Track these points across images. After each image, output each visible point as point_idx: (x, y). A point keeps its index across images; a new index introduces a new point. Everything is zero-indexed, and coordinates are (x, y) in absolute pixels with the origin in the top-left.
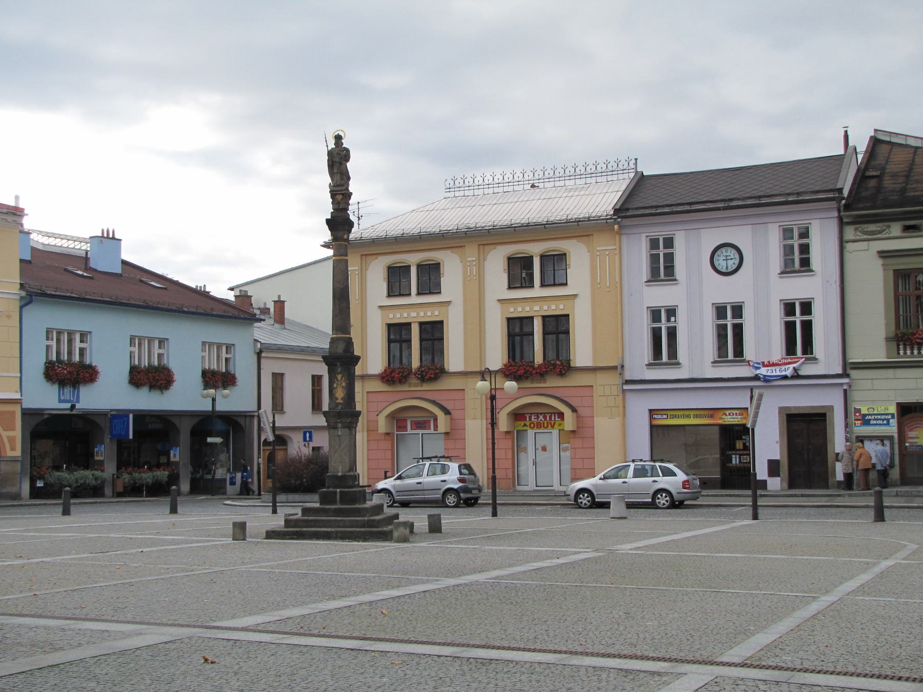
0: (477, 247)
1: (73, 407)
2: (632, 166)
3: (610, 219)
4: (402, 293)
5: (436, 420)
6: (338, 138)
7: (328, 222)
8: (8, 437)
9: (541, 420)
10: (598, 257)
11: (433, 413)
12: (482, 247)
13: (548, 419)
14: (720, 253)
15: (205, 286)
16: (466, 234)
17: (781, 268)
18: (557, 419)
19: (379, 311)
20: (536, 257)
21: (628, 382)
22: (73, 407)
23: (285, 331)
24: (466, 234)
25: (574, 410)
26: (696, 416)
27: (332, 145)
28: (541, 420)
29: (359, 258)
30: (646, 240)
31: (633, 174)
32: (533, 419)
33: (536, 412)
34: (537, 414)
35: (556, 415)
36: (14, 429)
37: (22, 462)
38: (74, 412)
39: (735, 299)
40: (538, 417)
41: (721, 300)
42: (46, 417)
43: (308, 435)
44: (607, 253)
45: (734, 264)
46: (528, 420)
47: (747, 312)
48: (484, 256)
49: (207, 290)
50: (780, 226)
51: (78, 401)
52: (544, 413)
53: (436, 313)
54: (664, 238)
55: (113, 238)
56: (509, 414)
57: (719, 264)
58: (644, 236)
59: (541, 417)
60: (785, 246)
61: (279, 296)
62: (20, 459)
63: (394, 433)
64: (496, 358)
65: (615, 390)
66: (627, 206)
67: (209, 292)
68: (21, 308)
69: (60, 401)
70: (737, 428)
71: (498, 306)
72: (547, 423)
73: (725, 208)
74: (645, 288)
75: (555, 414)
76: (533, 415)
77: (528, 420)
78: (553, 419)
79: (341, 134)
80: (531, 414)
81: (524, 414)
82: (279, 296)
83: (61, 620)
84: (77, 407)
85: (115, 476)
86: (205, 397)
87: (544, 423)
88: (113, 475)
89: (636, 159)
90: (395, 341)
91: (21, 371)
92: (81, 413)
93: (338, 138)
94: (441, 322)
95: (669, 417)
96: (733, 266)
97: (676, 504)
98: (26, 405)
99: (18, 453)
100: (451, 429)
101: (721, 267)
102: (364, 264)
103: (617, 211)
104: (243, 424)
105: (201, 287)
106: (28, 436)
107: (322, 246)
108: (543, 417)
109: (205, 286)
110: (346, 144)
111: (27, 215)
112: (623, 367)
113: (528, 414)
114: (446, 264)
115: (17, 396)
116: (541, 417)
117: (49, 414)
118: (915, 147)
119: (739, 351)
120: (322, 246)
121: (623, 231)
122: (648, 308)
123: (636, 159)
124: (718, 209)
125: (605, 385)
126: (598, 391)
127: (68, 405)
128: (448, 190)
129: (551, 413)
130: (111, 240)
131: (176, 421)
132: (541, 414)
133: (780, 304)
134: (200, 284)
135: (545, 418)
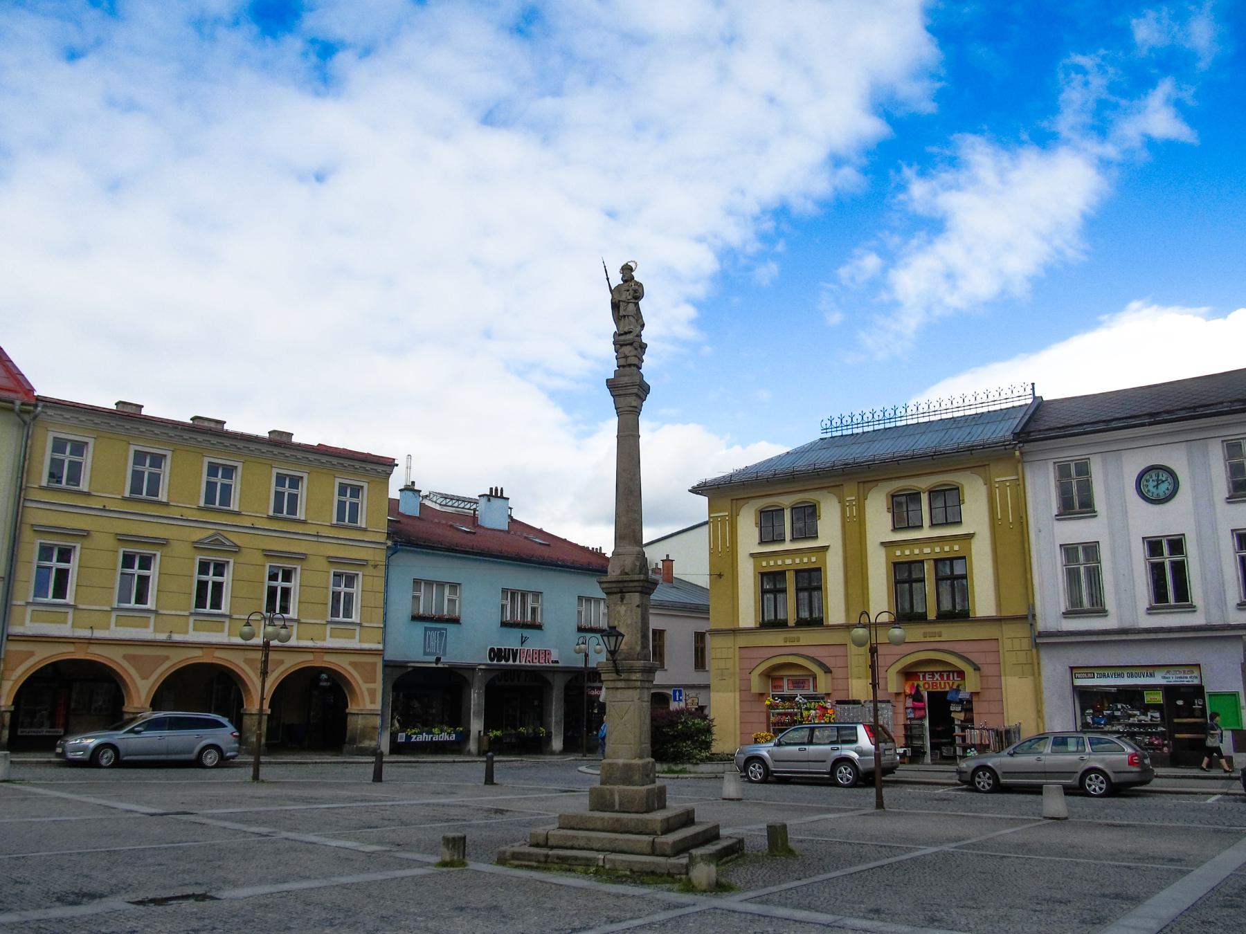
0: (856, 484)
1: (438, 660)
2: (1029, 391)
3: (1010, 444)
4: (775, 539)
5: (815, 678)
6: (627, 270)
7: (612, 385)
8: (368, 689)
9: (937, 679)
10: (997, 490)
11: (811, 671)
12: (861, 484)
13: (945, 679)
14: (1148, 477)
15: (601, 548)
16: (843, 471)
17: (1229, 492)
18: (956, 679)
19: (751, 560)
20: (924, 493)
21: (1041, 635)
22: (438, 660)
23: (673, 589)
24: (843, 471)
25: (977, 669)
26: (1131, 676)
27: (617, 280)
28: (937, 679)
29: (730, 502)
30: (1054, 469)
31: (1031, 400)
32: (927, 679)
33: (932, 670)
34: (933, 672)
35: (955, 675)
36: (374, 681)
37: (382, 715)
38: (440, 665)
39: (1174, 530)
40: (934, 676)
41: (1154, 532)
42: (409, 669)
43: (677, 694)
44: (1008, 484)
45: (1168, 489)
46: (921, 679)
47: (1191, 547)
48: (864, 492)
49: (603, 552)
50: (1223, 441)
51: (445, 654)
52: (941, 672)
53: (814, 559)
54: (1075, 464)
55: (502, 497)
56: (899, 672)
57: (1149, 491)
58: (1051, 464)
59: (937, 676)
60: (1231, 466)
61: (668, 556)
62: (380, 712)
63: (769, 694)
64: (880, 601)
65: (1026, 644)
66: (1027, 429)
67: (605, 554)
68: (388, 558)
69: (425, 653)
70: (1182, 690)
71: (882, 552)
72: (945, 683)
73: (1151, 424)
74: (1056, 523)
75: (953, 672)
76: (927, 675)
77: (921, 679)
78: (951, 678)
79: (633, 265)
80: (925, 672)
81: (916, 673)
82: (668, 556)
83: (608, 813)
84: (442, 660)
85: (482, 734)
86: (578, 652)
87: (940, 683)
88: (480, 732)
89: (1033, 384)
90: (769, 591)
91: (385, 622)
92: (447, 666)
93: (627, 270)
94: (819, 569)
95: (1096, 675)
96: (1167, 492)
97: (1117, 789)
98: (390, 656)
99: (378, 706)
100: (981, 689)
101: (1150, 494)
102: (734, 508)
103: (1016, 435)
104: (551, 681)
105: (597, 549)
106: (390, 687)
107: (689, 491)
108: (940, 676)
109: (601, 548)
110: (637, 276)
111: (397, 465)
112: (1034, 616)
113: (921, 672)
114: (822, 505)
115: (380, 647)
116: (937, 676)
117: (413, 667)
118: (1031, 607)
119: (1182, 593)
120: (689, 491)
121: (1026, 458)
122: (1061, 545)
123: (1033, 384)
124: (1143, 425)
125: (1013, 640)
126: (1006, 645)
127: (433, 658)
128: (825, 431)
129: (949, 672)
130: (500, 499)
131: (549, 677)
132: (937, 672)
133: (1233, 535)
134: (596, 546)
135: (941, 676)
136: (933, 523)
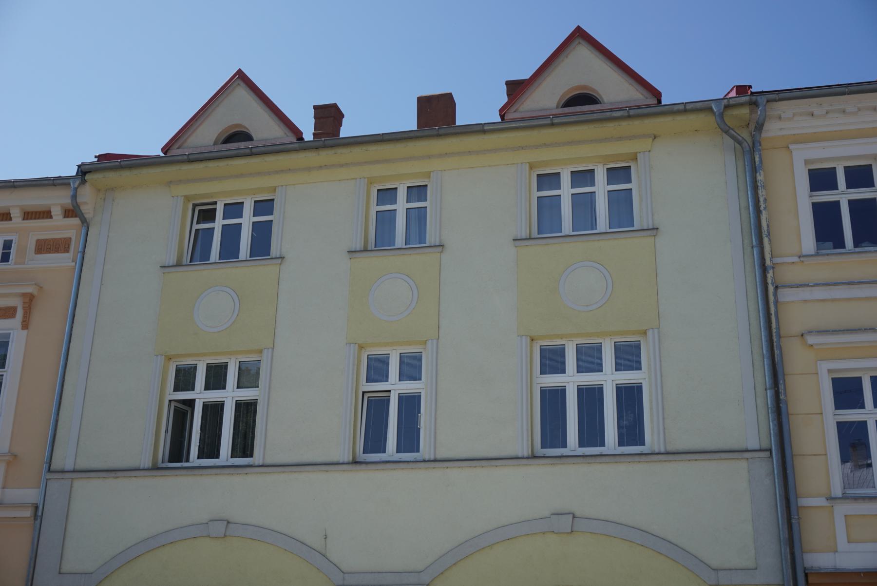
136: (241, 92)
